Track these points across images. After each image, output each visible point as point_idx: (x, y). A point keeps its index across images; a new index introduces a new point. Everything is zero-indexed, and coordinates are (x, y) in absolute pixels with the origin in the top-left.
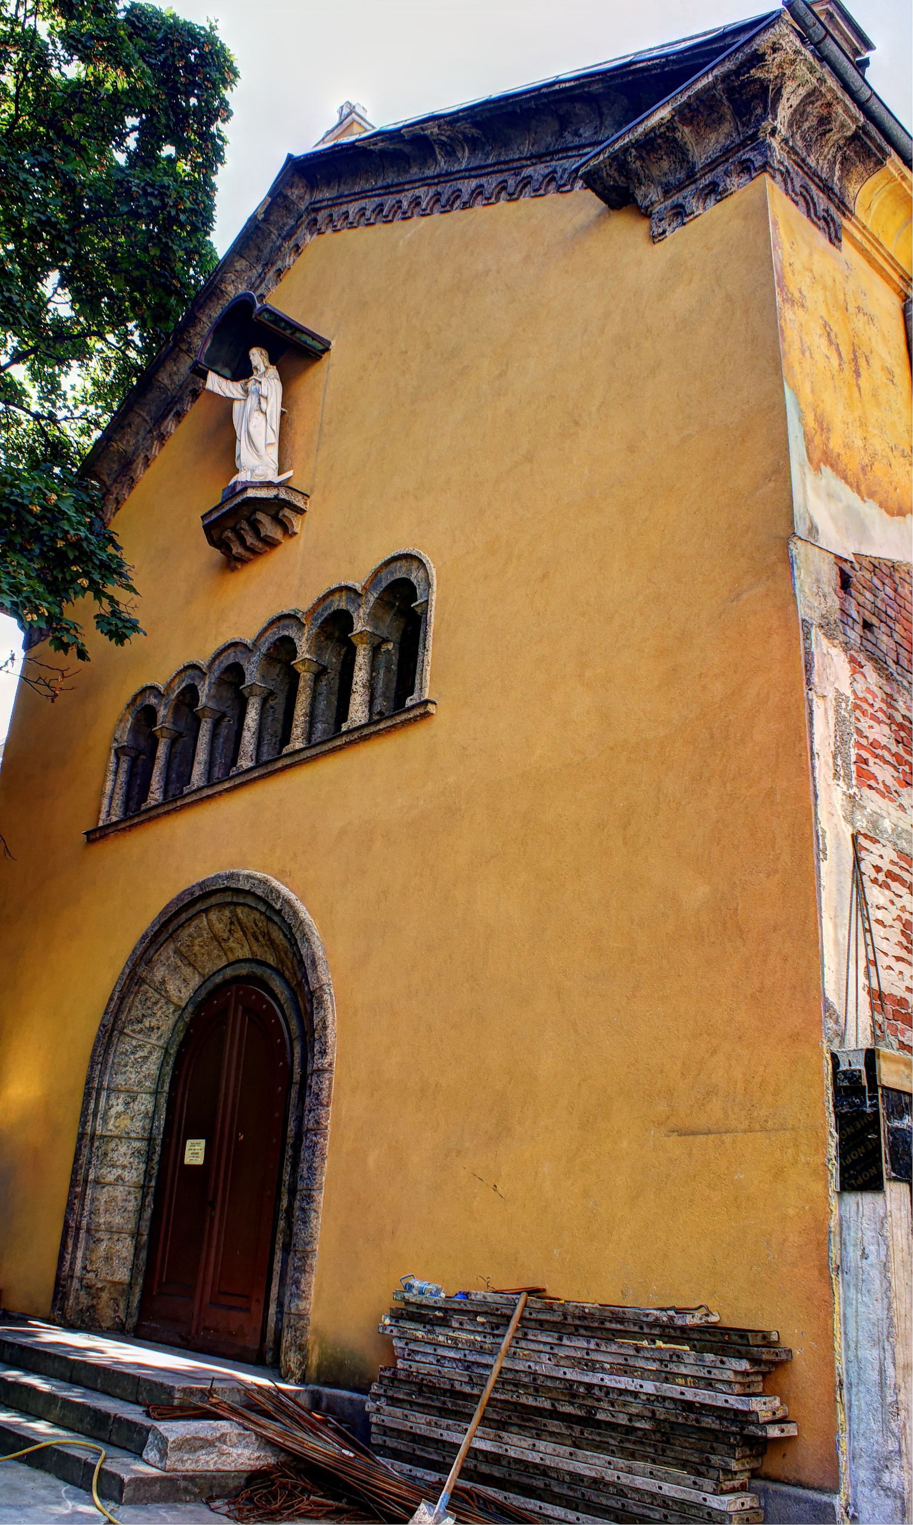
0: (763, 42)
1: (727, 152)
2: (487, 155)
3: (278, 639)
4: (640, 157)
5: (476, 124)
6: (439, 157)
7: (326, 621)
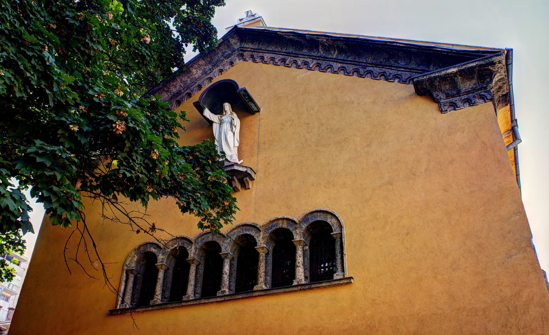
0: (496, 59)
1: (474, 90)
2: (348, 57)
3: (242, 235)
4: (439, 82)
5: (346, 44)
6: (320, 50)
7: (273, 232)
